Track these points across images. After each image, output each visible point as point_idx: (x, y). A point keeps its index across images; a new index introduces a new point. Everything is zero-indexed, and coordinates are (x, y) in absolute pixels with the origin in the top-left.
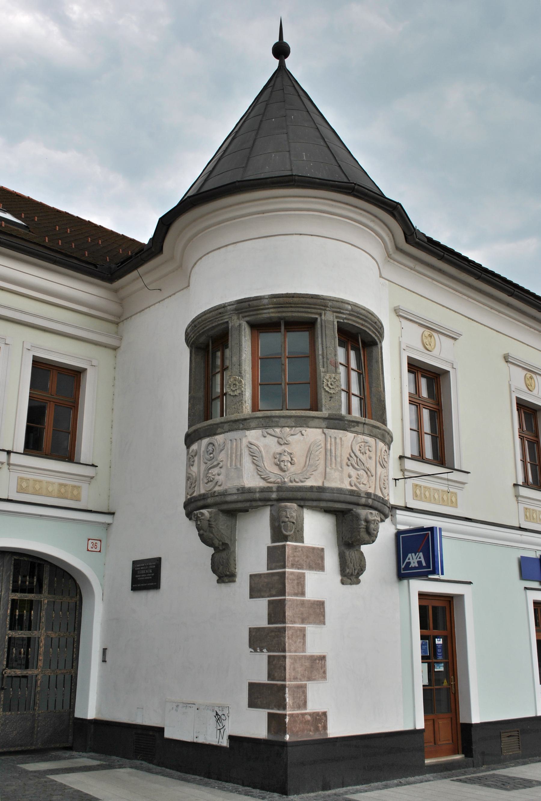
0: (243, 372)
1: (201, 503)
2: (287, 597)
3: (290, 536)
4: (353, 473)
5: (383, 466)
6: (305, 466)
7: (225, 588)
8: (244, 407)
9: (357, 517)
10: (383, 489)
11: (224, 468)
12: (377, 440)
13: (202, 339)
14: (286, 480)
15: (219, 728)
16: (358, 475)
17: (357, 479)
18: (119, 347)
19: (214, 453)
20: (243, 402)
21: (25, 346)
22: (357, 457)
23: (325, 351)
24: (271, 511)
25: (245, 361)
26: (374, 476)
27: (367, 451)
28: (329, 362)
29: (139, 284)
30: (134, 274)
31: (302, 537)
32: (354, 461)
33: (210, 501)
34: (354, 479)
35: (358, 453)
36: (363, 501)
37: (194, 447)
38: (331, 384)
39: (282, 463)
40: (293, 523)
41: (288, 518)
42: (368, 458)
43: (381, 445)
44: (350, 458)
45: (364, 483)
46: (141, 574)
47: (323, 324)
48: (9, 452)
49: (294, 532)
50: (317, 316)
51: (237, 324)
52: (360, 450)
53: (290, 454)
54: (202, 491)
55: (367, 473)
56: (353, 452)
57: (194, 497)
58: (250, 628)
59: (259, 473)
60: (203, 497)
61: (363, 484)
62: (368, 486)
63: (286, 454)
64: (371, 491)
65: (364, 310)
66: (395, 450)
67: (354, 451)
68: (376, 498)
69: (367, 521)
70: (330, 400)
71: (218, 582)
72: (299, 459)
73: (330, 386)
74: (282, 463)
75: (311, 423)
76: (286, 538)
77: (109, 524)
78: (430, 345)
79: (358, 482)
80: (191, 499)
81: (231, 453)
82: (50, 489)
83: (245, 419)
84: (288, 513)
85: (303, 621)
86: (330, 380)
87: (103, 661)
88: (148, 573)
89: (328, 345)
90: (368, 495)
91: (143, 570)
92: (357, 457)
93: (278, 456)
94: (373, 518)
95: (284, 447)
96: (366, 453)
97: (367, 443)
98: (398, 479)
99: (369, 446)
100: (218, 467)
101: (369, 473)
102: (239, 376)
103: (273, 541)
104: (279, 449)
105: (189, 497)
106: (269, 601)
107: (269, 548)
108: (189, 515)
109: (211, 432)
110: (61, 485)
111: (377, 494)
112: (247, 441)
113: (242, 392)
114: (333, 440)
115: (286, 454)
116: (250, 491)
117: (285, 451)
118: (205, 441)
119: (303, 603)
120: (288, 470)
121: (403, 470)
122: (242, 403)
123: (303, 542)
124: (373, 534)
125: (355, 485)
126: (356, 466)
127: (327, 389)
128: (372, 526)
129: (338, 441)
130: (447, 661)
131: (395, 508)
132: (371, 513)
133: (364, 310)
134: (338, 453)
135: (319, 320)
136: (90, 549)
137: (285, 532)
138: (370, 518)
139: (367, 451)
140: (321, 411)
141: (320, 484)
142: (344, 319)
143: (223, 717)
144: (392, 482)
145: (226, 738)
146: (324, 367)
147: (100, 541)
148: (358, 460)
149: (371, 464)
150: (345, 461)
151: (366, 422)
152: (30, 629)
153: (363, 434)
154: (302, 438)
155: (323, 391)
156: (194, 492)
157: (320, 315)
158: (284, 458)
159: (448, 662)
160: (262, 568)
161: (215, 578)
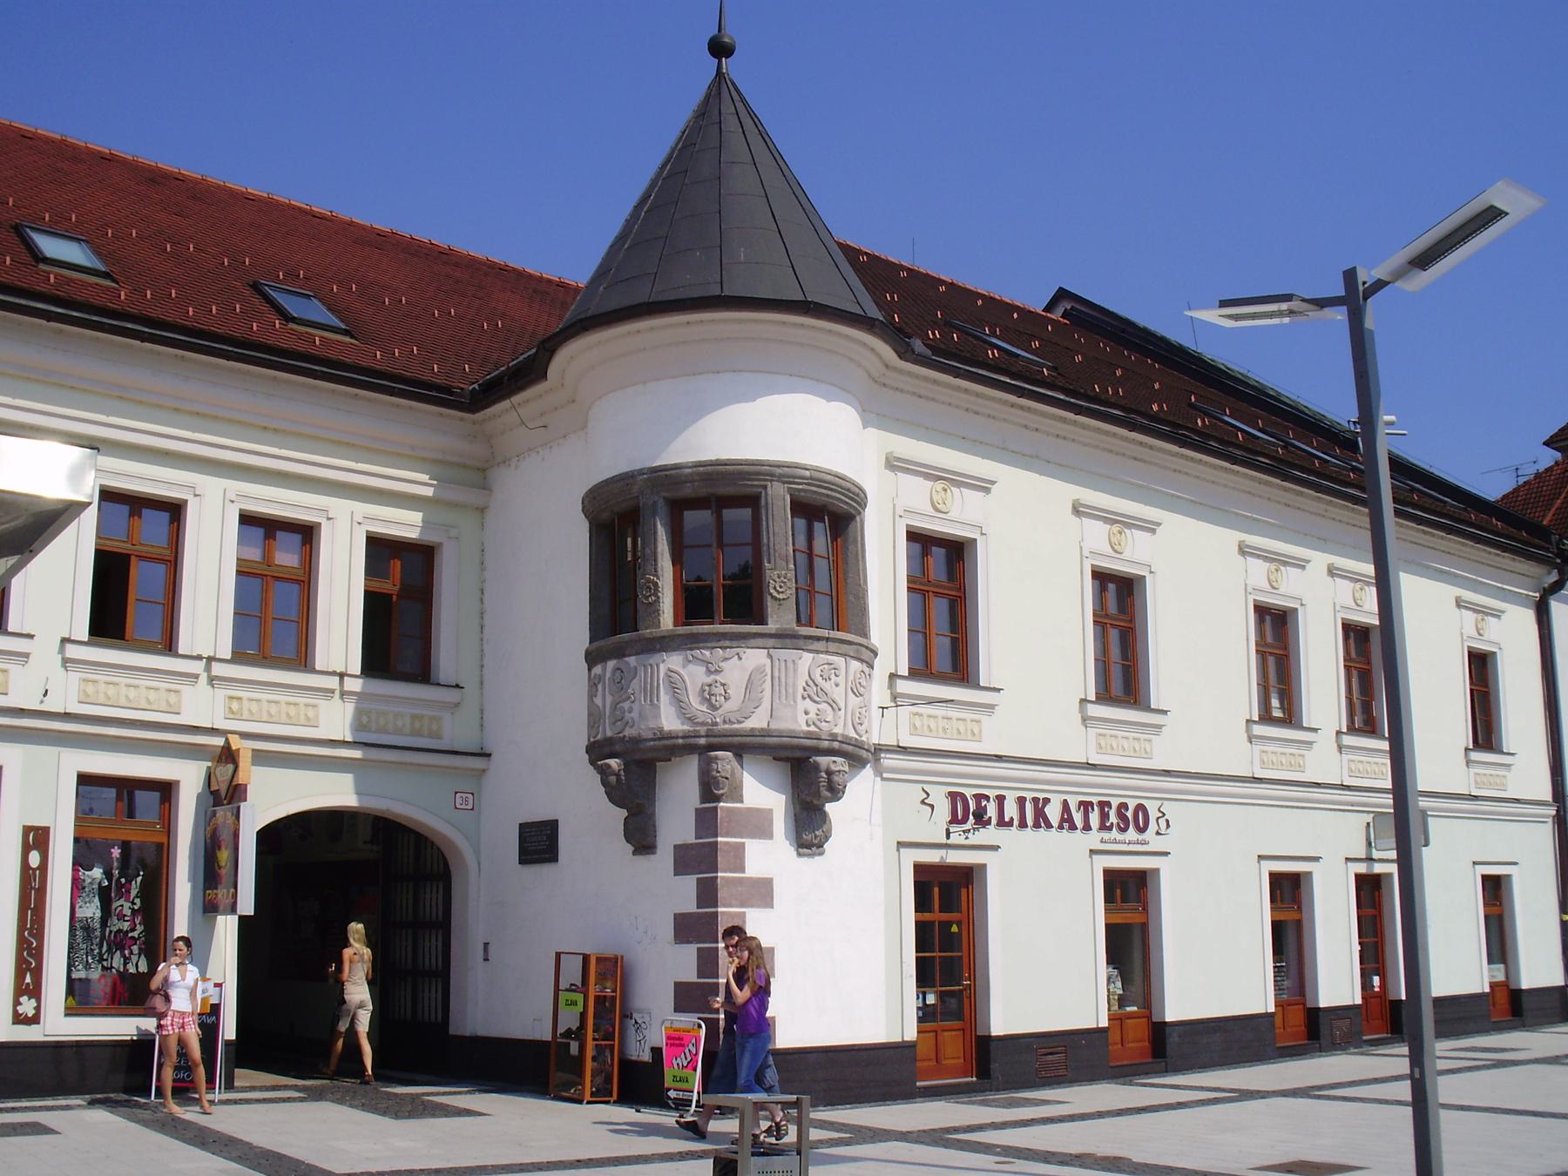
0: (659, 570)
1: (607, 750)
2: (719, 874)
3: (722, 795)
4: (812, 707)
5: (858, 694)
6: (743, 701)
7: (644, 861)
8: (661, 619)
9: (816, 767)
10: (859, 727)
11: (637, 703)
12: (848, 658)
13: (605, 516)
14: (718, 720)
15: (638, 1039)
16: (819, 710)
17: (817, 715)
18: (486, 508)
19: (623, 681)
20: (661, 612)
21: (354, 519)
22: (817, 685)
23: (772, 539)
24: (699, 761)
25: (662, 555)
26: (843, 710)
27: (833, 676)
28: (777, 555)
29: (512, 417)
30: (505, 404)
31: (742, 796)
32: (812, 691)
33: (618, 748)
34: (812, 715)
35: (819, 680)
36: (826, 744)
37: (597, 670)
38: (781, 587)
39: (713, 698)
40: (727, 778)
41: (719, 772)
42: (834, 686)
43: (855, 665)
44: (807, 688)
45: (827, 720)
46: (532, 842)
47: (770, 501)
48: (342, 676)
49: (729, 789)
50: (760, 490)
51: (651, 502)
52: (821, 676)
53: (723, 685)
54: (609, 734)
55: (832, 707)
56: (811, 679)
57: (598, 741)
58: (675, 914)
59: (683, 711)
60: (609, 741)
61: (826, 722)
62: (832, 724)
63: (718, 684)
64: (838, 730)
65: (830, 474)
66: (882, 666)
67: (813, 677)
68: (846, 740)
69: (829, 773)
70: (779, 609)
71: (634, 853)
72: (737, 693)
73: (778, 588)
74: (713, 698)
75: (753, 642)
76: (718, 799)
77: (484, 771)
78: (944, 503)
79: (819, 720)
80: (594, 742)
81: (645, 683)
82: (400, 724)
83: (664, 637)
84: (719, 766)
85: (742, 905)
86: (778, 580)
87: (485, 960)
88: (539, 841)
89: (776, 529)
90: (834, 737)
91: (535, 842)
92: (817, 685)
93: (707, 688)
94: (837, 769)
95: (713, 677)
96: (830, 679)
97: (831, 664)
98: (887, 708)
99: (835, 669)
100: (628, 702)
101: (834, 705)
102: (654, 575)
103: (702, 803)
104: (709, 680)
105: (592, 740)
106: (698, 879)
107: (697, 810)
108: (592, 762)
109: (619, 653)
110: (414, 717)
111: (847, 733)
112: (667, 667)
113: (658, 598)
114: (783, 664)
115: (718, 684)
116: (671, 736)
117: (716, 682)
118: (611, 664)
119: (741, 880)
120: (721, 706)
121: (894, 697)
122: (659, 614)
123: (742, 802)
124: (839, 789)
125: (814, 724)
126: (818, 699)
127: (775, 594)
128: (836, 778)
129: (790, 665)
130: (1376, 940)
131: (879, 750)
132: (834, 762)
133: (830, 474)
134: (790, 681)
135: (763, 494)
136: (458, 806)
137: (716, 792)
138: (833, 767)
139: (833, 676)
140: (767, 624)
141: (764, 725)
142: (800, 490)
143: (643, 1025)
144: (876, 713)
145: (647, 1050)
146: (769, 562)
147: (473, 794)
148: (819, 690)
149: (838, 694)
150: (800, 691)
151: (831, 636)
152: (692, 1092)
153: (827, 652)
154: (738, 662)
155: (769, 597)
156: (598, 733)
157: (765, 487)
158: (715, 690)
159: (961, 957)
160: (689, 836)
161: (630, 848)
